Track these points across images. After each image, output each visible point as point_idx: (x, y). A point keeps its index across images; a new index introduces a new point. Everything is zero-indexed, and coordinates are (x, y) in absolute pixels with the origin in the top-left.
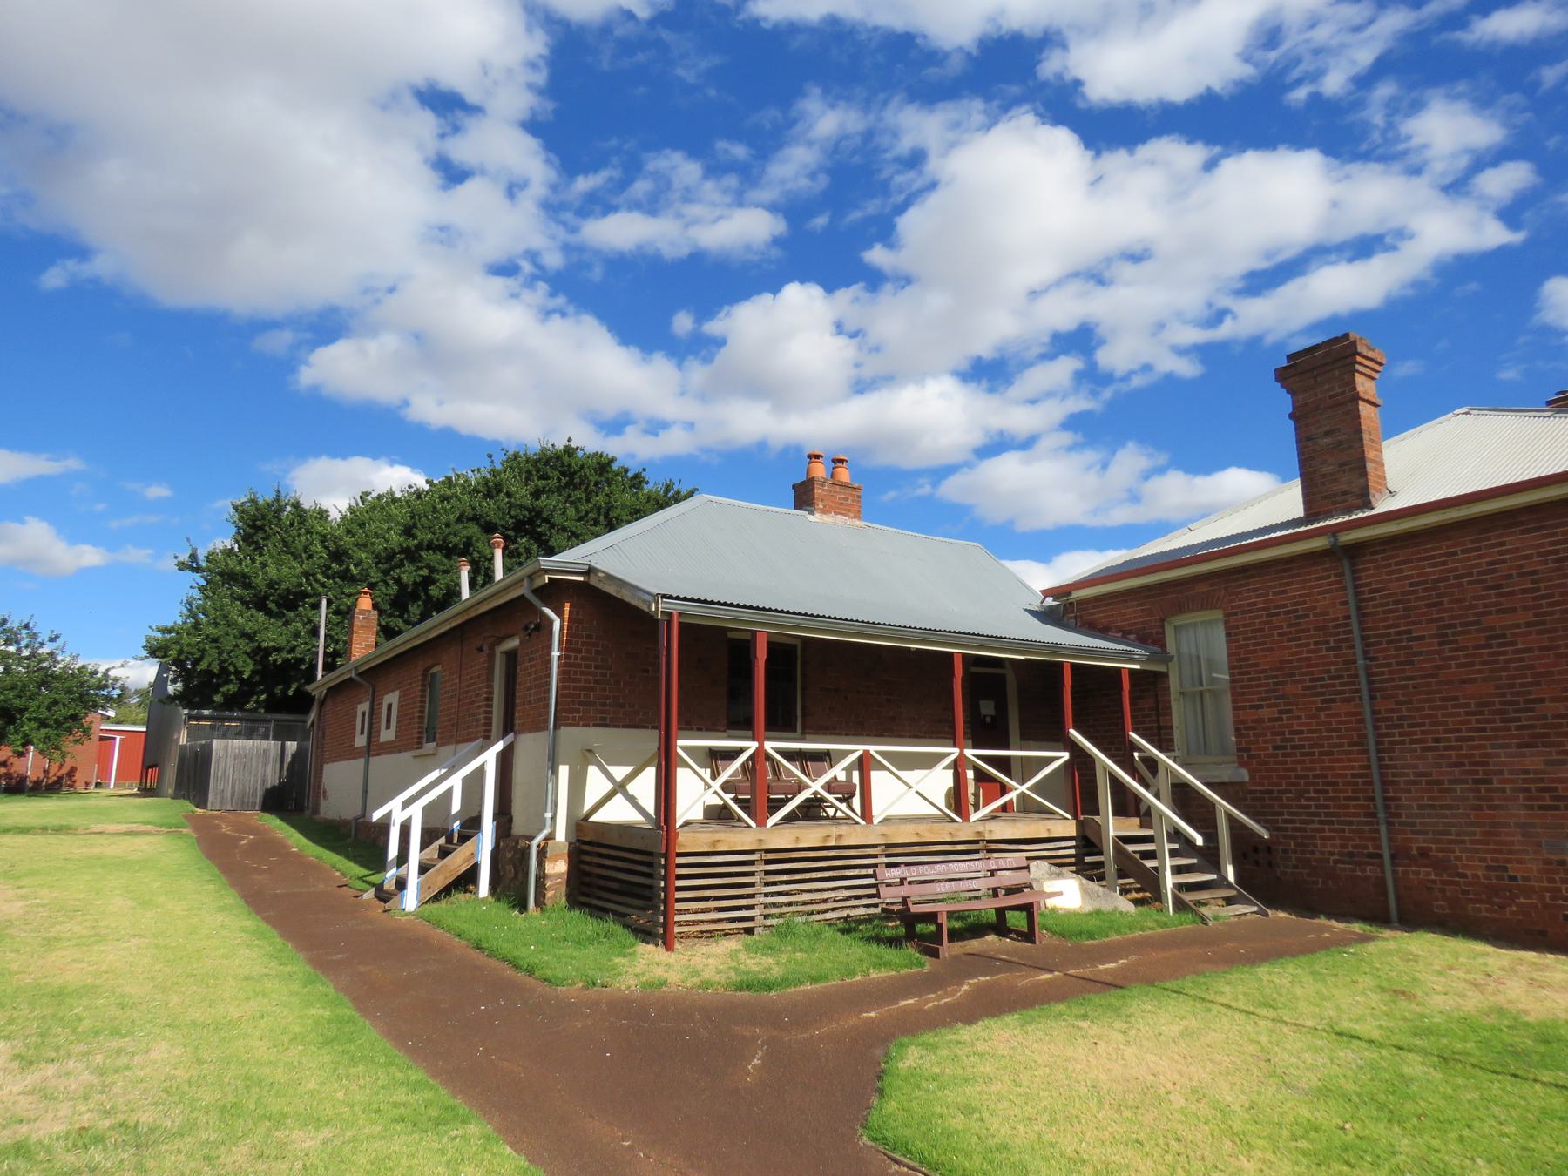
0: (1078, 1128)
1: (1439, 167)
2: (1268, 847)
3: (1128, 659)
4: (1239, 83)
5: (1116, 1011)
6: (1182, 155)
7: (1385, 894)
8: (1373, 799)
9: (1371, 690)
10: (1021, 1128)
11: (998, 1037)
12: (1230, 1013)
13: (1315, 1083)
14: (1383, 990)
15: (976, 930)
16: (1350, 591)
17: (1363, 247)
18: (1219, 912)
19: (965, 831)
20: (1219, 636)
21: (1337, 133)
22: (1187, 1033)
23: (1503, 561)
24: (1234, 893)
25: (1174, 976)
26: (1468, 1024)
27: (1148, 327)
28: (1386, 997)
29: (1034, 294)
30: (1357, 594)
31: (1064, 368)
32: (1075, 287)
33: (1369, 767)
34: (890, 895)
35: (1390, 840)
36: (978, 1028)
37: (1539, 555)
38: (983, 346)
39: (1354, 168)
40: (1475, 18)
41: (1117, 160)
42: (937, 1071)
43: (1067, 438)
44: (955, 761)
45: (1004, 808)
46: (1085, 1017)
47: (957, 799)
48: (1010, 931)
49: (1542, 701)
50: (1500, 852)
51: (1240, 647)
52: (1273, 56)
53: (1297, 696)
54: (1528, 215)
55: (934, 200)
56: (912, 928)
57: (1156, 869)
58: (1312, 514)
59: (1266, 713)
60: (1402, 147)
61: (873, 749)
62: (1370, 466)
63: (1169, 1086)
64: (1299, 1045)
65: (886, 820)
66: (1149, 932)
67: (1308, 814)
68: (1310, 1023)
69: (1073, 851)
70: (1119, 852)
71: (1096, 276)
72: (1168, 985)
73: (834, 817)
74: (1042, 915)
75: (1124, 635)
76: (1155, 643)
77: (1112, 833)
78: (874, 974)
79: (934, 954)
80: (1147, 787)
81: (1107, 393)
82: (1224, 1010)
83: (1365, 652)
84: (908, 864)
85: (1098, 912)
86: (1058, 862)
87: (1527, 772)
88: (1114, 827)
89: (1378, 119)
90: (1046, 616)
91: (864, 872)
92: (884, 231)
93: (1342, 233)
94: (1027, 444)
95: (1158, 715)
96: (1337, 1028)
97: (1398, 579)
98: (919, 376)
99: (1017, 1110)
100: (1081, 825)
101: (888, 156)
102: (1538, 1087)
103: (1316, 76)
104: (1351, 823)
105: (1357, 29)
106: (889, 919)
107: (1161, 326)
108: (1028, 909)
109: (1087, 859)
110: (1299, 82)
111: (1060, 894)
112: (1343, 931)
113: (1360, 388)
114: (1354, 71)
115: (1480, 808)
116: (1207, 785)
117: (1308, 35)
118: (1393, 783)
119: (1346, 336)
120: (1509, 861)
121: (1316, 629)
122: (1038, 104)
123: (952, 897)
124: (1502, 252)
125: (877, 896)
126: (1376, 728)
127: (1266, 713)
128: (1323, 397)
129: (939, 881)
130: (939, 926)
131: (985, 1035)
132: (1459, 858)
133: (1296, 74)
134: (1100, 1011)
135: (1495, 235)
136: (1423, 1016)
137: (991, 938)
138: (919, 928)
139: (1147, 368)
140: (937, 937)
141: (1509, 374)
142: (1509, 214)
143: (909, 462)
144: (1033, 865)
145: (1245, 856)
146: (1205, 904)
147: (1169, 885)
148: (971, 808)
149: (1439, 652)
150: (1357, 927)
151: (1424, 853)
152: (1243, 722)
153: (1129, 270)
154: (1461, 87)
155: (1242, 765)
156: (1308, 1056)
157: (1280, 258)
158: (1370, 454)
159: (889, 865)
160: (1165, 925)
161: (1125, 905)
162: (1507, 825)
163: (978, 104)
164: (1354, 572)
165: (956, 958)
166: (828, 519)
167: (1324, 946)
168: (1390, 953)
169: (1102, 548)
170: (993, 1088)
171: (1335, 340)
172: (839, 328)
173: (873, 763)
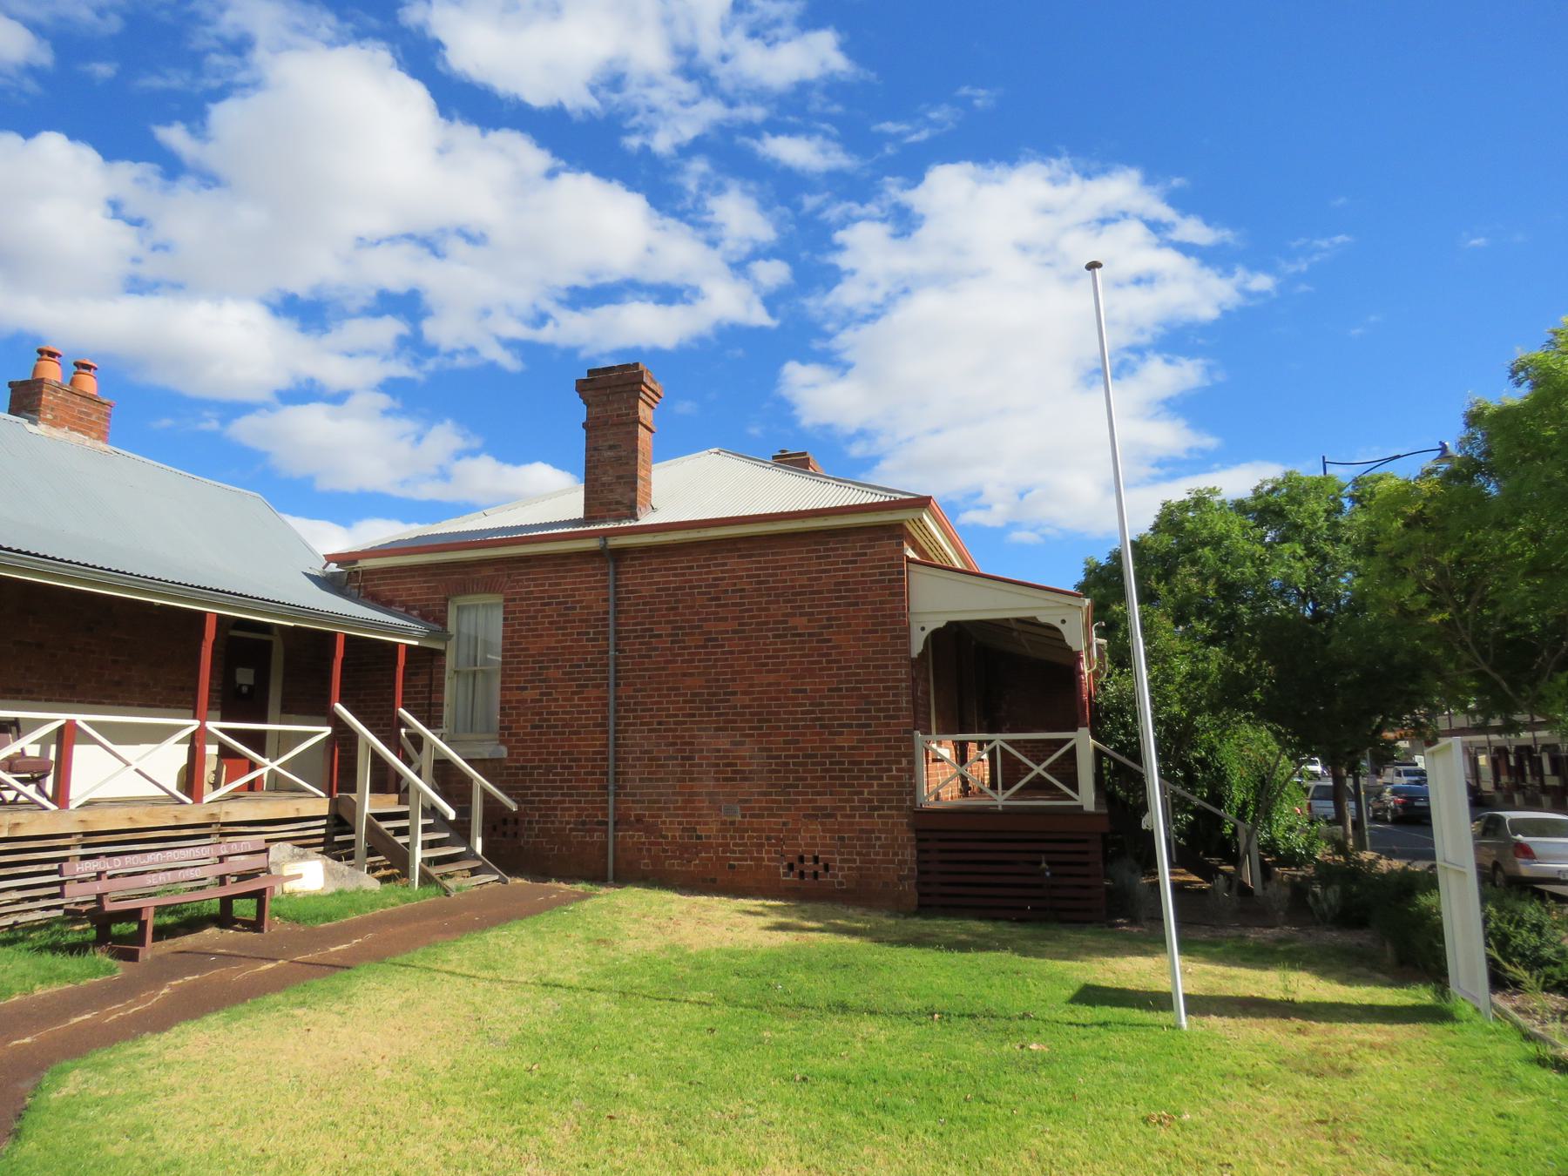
0: (269, 1123)
1: (730, 245)
2: (516, 819)
3: (406, 634)
4: (586, 112)
5: (338, 994)
6: (522, 154)
7: (606, 856)
8: (606, 773)
9: (616, 678)
10: (200, 1138)
11: (196, 1040)
12: (453, 979)
13: (516, 1032)
14: (589, 940)
15: (194, 924)
16: (611, 590)
17: (668, 294)
18: (462, 883)
19: (193, 813)
20: (498, 616)
21: (655, 182)
22: (408, 1004)
23: (723, 579)
24: (479, 864)
25: (406, 950)
26: (647, 961)
27: (478, 308)
28: (590, 946)
29: (361, 242)
30: (616, 593)
31: (389, 329)
32: (407, 248)
33: (606, 746)
34: (77, 894)
35: (616, 809)
36: (168, 1037)
37: (748, 576)
38: (299, 284)
39: (671, 222)
40: (766, 134)
41: (466, 135)
42: (104, 1093)
43: (383, 400)
44: (193, 734)
45: (251, 786)
46: (302, 1004)
47: (190, 780)
48: (236, 921)
49: (734, 693)
50: (693, 816)
51: (514, 631)
52: (616, 98)
53: (556, 680)
54: (781, 307)
55: (256, 100)
56: (110, 930)
57: (407, 845)
58: (589, 518)
59: (529, 694)
60: (707, 218)
61: (80, 719)
62: (640, 483)
63: (378, 1060)
64: (510, 999)
65: (89, 804)
66: (390, 909)
67: (554, 788)
68: (523, 979)
69: (322, 831)
70: (372, 829)
71: (430, 244)
72: (398, 960)
73: (14, 802)
74: (278, 900)
75: (407, 610)
76: (436, 620)
77: (367, 810)
78: (40, 991)
79: (132, 957)
80: (409, 763)
81: (430, 365)
82: (447, 977)
83: (616, 645)
84: (109, 855)
85: (340, 893)
86: (303, 843)
87: (718, 751)
88: (368, 803)
89: (692, 185)
90: (327, 583)
91: (46, 867)
92: (193, 112)
93: (651, 277)
94: (338, 398)
95: (430, 692)
96: (545, 980)
97: (650, 584)
98: (219, 293)
99: (199, 1119)
100: (334, 804)
101: (210, 30)
102: (687, 1006)
103: (648, 131)
104: (586, 795)
105: (684, 104)
106: (76, 921)
107: (486, 313)
108: (259, 895)
109: (337, 839)
110: (633, 131)
111: (299, 876)
112: (569, 892)
113: (641, 414)
114: (678, 139)
115: (684, 780)
116: (468, 761)
117: (646, 91)
118: (624, 759)
119: (636, 365)
120: (698, 823)
121: (581, 621)
122: (397, 47)
123: (169, 889)
124: (761, 330)
125: (60, 895)
126: (616, 711)
127: (529, 694)
128: (612, 409)
129: (154, 872)
130: (143, 925)
131: (178, 1041)
132: (664, 823)
133: (633, 122)
134: (320, 995)
135: (759, 317)
136: (615, 959)
137: (211, 932)
138: (116, 929)
139: (472, 351)
140: (139, 938)
141: (755, 431)
142: (771, 301)
143: (194, 389)
144: (273, 848)
145: (495, 828)
146: (451, 877)
147: (418, 860)
148: (207, 787)
149: (670, 649)
150: (580, 887)
151: (639, 819)
152: (510, 702)
153: (459, 247)
154: (752, 186)
155: (502, 742)
156: (514, 1010)
157: (600, 281)
158: (641, 473)
159: (84, 858)
160: (409, 900)
161: (371, 883)
162: (700, 794)
163: (330, 19)
164: (616, 573)
165: (159, 959)
166: (57, 433)
167: (549, 906)
168: (601, 907)
169: (407, 520)
170: (175, 1100)
171: (626, 367)
172: (115, 208)
173: (78, 733)
